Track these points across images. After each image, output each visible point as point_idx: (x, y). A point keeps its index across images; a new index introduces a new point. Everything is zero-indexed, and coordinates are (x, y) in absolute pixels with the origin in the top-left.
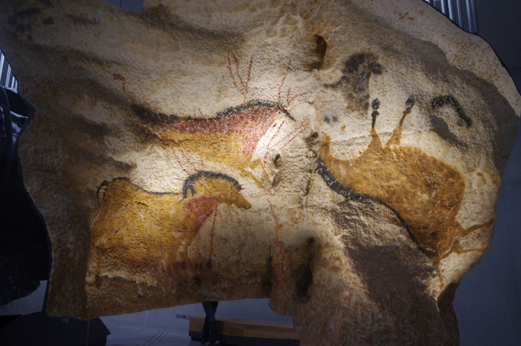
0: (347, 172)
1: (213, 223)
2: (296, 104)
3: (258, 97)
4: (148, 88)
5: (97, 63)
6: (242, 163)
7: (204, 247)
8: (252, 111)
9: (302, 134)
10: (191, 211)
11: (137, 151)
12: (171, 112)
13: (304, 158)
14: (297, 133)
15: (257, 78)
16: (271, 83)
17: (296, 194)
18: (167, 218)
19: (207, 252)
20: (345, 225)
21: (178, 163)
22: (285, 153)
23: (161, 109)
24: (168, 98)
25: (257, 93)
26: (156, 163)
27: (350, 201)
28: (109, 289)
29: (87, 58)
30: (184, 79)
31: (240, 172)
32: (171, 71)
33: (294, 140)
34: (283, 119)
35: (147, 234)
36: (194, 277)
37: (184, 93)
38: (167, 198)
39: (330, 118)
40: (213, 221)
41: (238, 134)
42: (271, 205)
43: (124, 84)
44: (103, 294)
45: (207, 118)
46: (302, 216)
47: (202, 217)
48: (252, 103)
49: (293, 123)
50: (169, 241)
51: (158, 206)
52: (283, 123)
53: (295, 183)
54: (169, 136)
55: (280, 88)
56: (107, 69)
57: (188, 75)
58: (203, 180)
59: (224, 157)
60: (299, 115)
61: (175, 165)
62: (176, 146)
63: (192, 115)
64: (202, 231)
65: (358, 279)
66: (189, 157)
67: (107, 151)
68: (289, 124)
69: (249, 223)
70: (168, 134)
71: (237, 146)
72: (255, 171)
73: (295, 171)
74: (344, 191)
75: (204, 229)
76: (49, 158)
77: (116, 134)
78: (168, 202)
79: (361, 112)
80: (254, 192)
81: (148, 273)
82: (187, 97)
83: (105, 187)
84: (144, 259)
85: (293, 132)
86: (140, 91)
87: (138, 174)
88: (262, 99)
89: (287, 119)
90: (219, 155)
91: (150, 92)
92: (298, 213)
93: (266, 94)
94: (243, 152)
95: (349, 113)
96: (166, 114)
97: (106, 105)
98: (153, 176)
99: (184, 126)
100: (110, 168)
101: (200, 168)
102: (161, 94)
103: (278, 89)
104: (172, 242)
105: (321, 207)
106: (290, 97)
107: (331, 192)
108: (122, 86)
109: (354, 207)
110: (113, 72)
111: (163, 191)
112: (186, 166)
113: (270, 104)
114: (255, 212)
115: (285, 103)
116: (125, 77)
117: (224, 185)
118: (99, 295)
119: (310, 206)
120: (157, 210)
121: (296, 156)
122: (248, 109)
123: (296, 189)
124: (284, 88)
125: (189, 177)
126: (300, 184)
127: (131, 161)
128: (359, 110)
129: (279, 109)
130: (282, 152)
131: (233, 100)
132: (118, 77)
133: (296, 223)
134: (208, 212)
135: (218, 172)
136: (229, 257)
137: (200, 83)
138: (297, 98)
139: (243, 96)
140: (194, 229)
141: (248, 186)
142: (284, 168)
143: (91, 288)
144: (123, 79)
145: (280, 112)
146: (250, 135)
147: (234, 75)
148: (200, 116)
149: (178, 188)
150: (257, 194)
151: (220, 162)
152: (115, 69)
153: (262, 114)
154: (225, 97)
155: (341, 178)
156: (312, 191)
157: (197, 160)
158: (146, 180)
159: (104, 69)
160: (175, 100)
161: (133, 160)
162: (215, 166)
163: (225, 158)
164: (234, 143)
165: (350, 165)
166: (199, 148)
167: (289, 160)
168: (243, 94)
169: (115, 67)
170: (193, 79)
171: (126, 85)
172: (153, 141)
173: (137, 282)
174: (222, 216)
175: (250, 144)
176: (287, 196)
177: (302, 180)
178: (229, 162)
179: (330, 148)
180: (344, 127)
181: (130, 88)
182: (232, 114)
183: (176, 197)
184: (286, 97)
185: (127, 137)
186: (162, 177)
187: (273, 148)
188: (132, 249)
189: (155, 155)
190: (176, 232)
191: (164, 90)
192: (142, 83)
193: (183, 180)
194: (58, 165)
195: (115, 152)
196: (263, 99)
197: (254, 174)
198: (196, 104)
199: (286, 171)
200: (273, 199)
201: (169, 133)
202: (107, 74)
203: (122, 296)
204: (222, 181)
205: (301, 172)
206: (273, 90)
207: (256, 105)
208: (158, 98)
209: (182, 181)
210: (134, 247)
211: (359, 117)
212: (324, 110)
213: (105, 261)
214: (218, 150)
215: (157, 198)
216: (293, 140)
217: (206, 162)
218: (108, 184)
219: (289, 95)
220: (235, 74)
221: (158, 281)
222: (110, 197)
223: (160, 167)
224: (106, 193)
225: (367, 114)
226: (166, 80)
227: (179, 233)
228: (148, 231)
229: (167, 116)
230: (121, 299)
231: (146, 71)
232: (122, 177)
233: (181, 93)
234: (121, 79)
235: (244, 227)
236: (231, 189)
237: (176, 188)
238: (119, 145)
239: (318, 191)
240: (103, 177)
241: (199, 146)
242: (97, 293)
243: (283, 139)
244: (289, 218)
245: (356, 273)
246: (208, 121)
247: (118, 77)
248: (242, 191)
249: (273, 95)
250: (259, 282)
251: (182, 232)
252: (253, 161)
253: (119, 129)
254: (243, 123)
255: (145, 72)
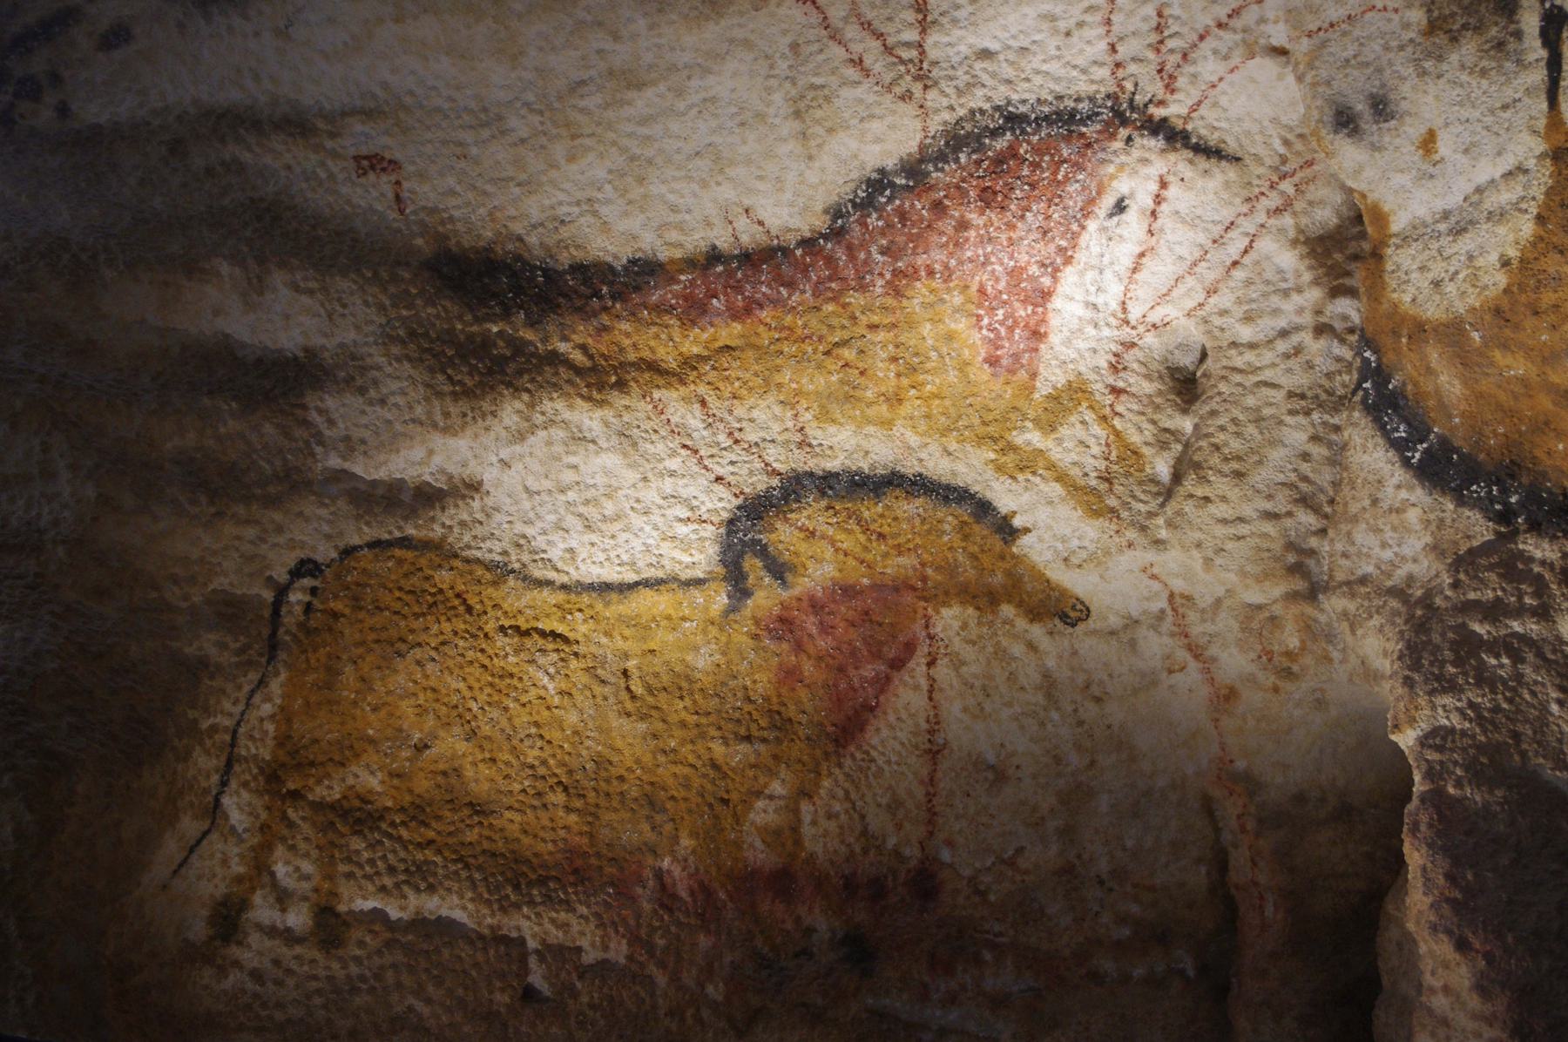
0: (1465, 383)
1: (931, 699)
2: (1214, 79)
3: (1000, 94)
4: (504, 174)
5: (291, 135)
6: (996, 414)
7: (895, 806)
8: (978, 163)
9: (1287, 220)
10: (799, 647)
11: (447, 430)
12: (629, 250)
13: (1306, 337)
14: (1261, 217)
15: (970, 9)
16: (1058, 10)
17: (1269, 528)
18: (682, 684)
19: (907, 826)
20: (1452, 670)
21: (684, 452)
22: (1217, 333)
23: (578, 247)
24: (600, 196)
25: (993, 75)
26: (575, 467)
27: (1521, 538)
28: (377, 961)
29: (256, 125)
30: (643, 102)
31: (992, 456)
32: (583, 83)
33: (1252, 256)
34: (1159, 166)
35: (584, 753)
36: (840, 935)
37: (659, 160)
38: (645, 602)
39: (1360, 107)
40: (925, 688)
41: (937, 283)
42: (1172, 596)
43: (398, 183)
44: (348, 976)
45: (791, 239)
46: (1315, 638)
47: (868, 671)
48: (968, 127)
49: (1223, 174)
50: (697, 782)
51: (625, 638)
52: (1164, 185)
53: (1261, 477)
54: (630, 349)
55: (1108, 22)
56: (329, 144)
57: (654, 83)
58: (812, 513)
59: (896, 400)
60: (1255, 128)
61: (674, 464)
62: (669, 385)
63: (723, 242)
64: (885, 733)
65: (1464, 970)
66: (740, 420)
67: (318, 450)
68: (1200, 183)
69: (1096, 690)
70: (627, 342)
71: (950, 337)
72: (1059, 441)
73: (1267, 412)
74: (1489, 486)
75: (892, 728)
76: (21, 503)
77: (349, 380)
78: (669, 618)
79: (1494, 31)
80: (1075, 543)
81: (583, 910)
82: (677, 174)
83: (307, 582)
84: (572, 852)
85: (1241, 220)
86: (470, 195)
87: (498, 517)
88: (1026, 96)
89: (1179, 163)
90: (869, 394)
91: (517, 190)
92: (1290, 627)
93: (1045, 67)
94: (986, 360)
95: (1440, 58)
96: (609, 259)
97: (306, 279)
98: (571, 521)
99: (700, 293)
100: (323, 512)
101: (785, 460)
102: (567, 186)
103: (1102, 30)
104: (709, 787)
105: (1389, 583)
106: (1172, 51)
107: (1428, 500)
108: (391, 195)
109: (1537, 569)
110: (352, 151)
111: (631, 577)
112: (725, 462)
113: (1072, 114)
114: (1112, 633)
115: (1152, 87)
116: (398, 156)
117: (923, 521)
118: (330, 978)
119: (1341, 584)
120: (626, 656)
121: (1272, 334)
122: (957, 160)
123: (1268, 506)
124: (1131, 14)
125: (739, 508)
126: (1293, 477)
127: (442, 471)
128: (1478, 29)
129: (1125, 122)
130: (1202, 328)
131: (869, 137)
132: (373, 163)
133: (1288, 674)
134: (891, 652)
135: (885, 467)
136: (1020, 850)
137: (713, 100)
138: (1206, 46)
139: (909, 109)
140: (830, 729)
141: (1042, 515)
142: (1213, 405)
143: (298, 950)
144: (394, 164)
145: (1129, 139)
146: (994, 277)
147: (840, 25)
148: (763, 239)
149: (698, 557)
150: (1092, 547)
151: (887, 424)
152: (362, 136)
153: (1035, 166)
154: (830, 131)
155: (1450, 417)
156: (1346, 504)
157: (776, 427)
158: (539, 538)
159: (318, 148)
160: (630, 196)
161: (452, 469)
162: (864, 444)
163: (900, 401)
164: (928, 326)
165: (1469, 338)
166: (778, 378)
167: (1239, 362)
168: (902, 98)
169: (359, 128)
170: (680, 93)
171: (406, 185)
172: (533, 380)
173: (532, 944)
174: (963, 663)
175: (1006, 318)
176: (1230, 546)
177: (1305, 456)
178: (928, 416)
179: (1389, 267)
180: (1428, 142)
181: (423, 193)
182: (890, 199)
183: (698, 596)
184: (1151, 55)
185: (395, 385)
186: (617, 517)
187: (1154, 316)
188: (508, 814)
189: (558, 433)
190: (726, 744)
191: (574, 167)
192: (477, 162)
193: (716, 519)
194: (56, 523)
195: (349, 446)
196: (1032, 98)
197: (1056, 454)
198: (727, 193)
199: (1222, 421)
200: (1172, 561)
201: (628, 335)
202: (330, 163)
203: (430, 989)
204: (910, 507)
205: (1292, 412)
206: (1074, 39)
207: (995, 133)
208: (560, 203)
209: (711, 528)
210: (516, 805)
211: (1484, 63)
212: (1324, 74)
213: (366, 855)
214: (862, 373)
215: (607, 604)
216: (1247, 260)
217: (819, 433)
218: (321, 571)
219: (1161, 42)
220: (845, 19)
221: (629, 944)
222: (336, 615)
223: (600, 480)
224: (317, 603)
225: (1518, 35)
226: (567, 125)
227: (743, 748)
228: (588, 743)
229: (611, 268)
230: (428, 1001)
231: (485, 110)
232: (386, 536)
233: (650, 162)
234: (384, 170)
235: (1070, 709)
236: (966, 537)
237: (687, 559)
238: (364, 420)
239: (1367, 503)
240: (292, 545)
241: (778, 369)
242: (322, 973)
243: (1195, 264)
244: (1253, 655)
245: (1449, 932)
246: (799, 252)
247: (373, 163)
248: (1025, 541)
249: (1080, 61)
250: (1191, 973)
251: (764, 740)
252: (1049, 397)
253: (362, 359)
254: (950, 230)
255: (482, 116)
